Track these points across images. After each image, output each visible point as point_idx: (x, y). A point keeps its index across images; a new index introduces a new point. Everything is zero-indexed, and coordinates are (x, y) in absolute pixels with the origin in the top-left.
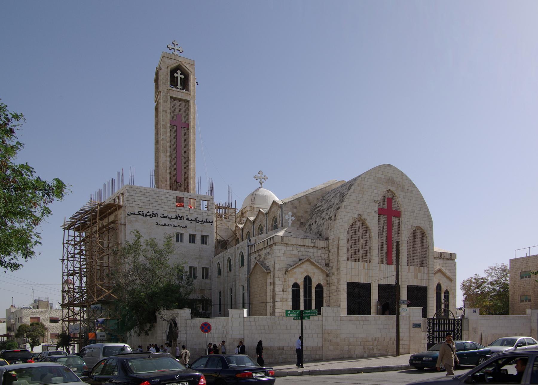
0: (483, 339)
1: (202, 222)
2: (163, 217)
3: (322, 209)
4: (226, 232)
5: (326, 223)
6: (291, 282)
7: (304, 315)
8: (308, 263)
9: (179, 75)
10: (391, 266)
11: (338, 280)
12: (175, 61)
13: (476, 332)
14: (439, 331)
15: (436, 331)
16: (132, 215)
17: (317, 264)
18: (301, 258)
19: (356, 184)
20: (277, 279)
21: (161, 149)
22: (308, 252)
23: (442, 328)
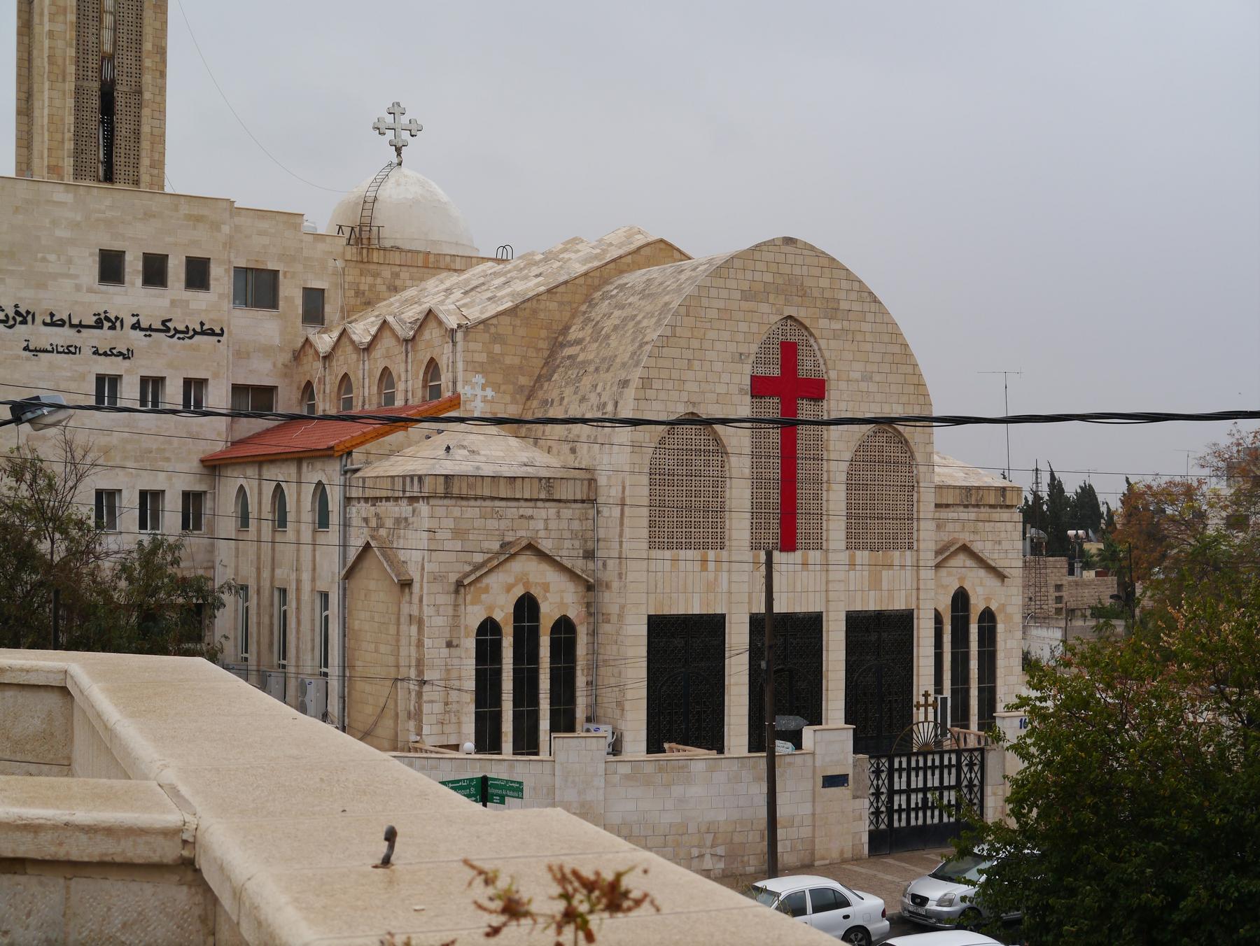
1: (187, 333)
2: (53, 324)
3: (580, 358)
6: (474, 617)
7: (491, 791)
11: (622, 607)
15: (900, 792)
18: (507, 539)
21: (41, 62)
22: (531, 517)
23: (916, 782)
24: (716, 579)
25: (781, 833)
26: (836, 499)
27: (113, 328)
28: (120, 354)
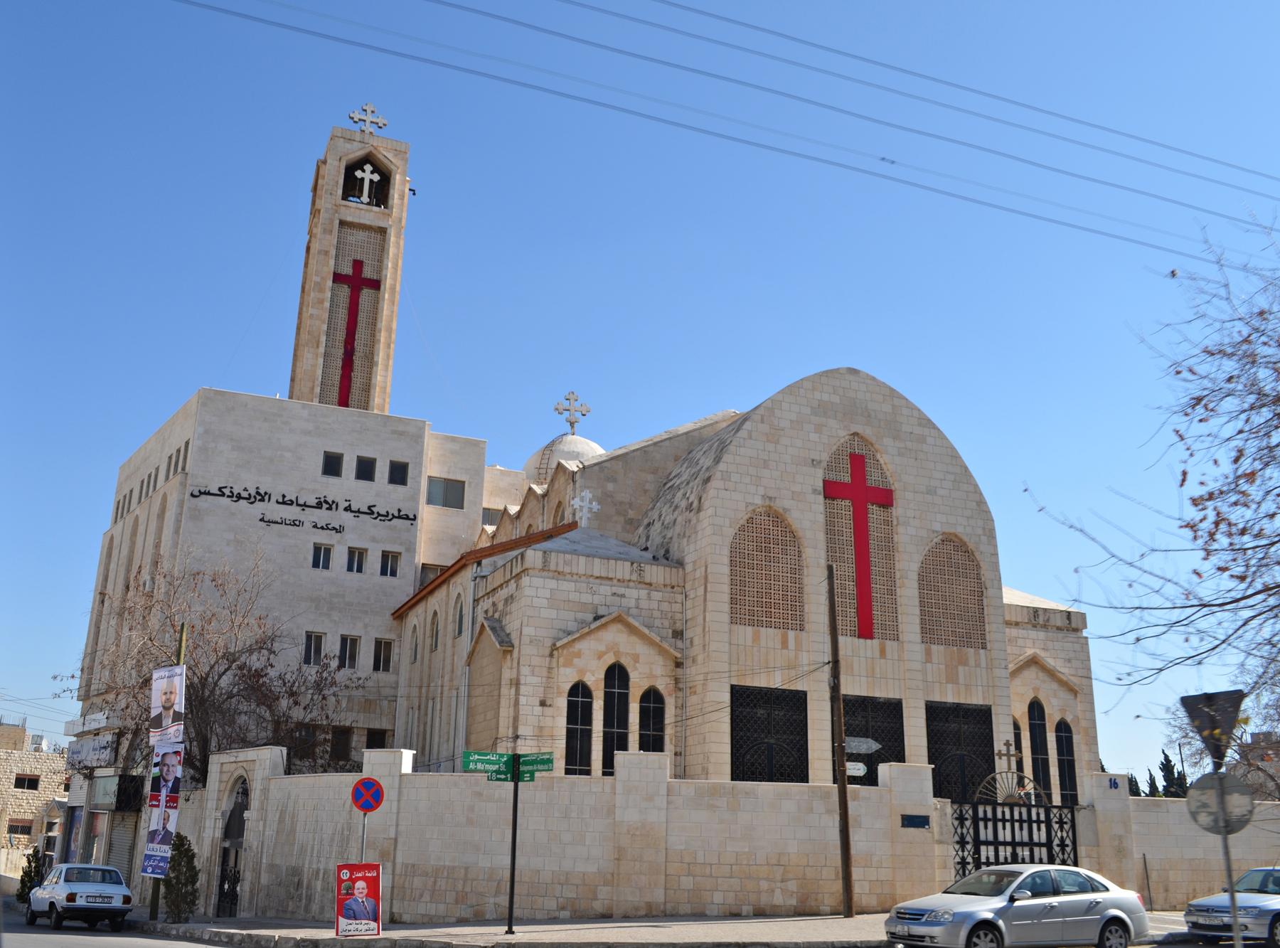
0: (1154, 876)
1: (386, 516)
2: (284, 503)
4: (454, 544)
5: (679, 519)
6: (567, 677)
7: (522, 768)
8: (619, 626)
9: (367, 175)
10: (869, 641)
12: (360, 145)
13: (1121, 852)
14: (996, 843)
16: (203, 497)
17: (646, 631)
18: (600, 613)
19: (756, 417)
20: (525, 670)
22: (623, 596)
23: (1005, 834)
24: (796, 657)
25: (856, 873)
26: (908, 595)
27: (330, 509)
28: (334, 528)
